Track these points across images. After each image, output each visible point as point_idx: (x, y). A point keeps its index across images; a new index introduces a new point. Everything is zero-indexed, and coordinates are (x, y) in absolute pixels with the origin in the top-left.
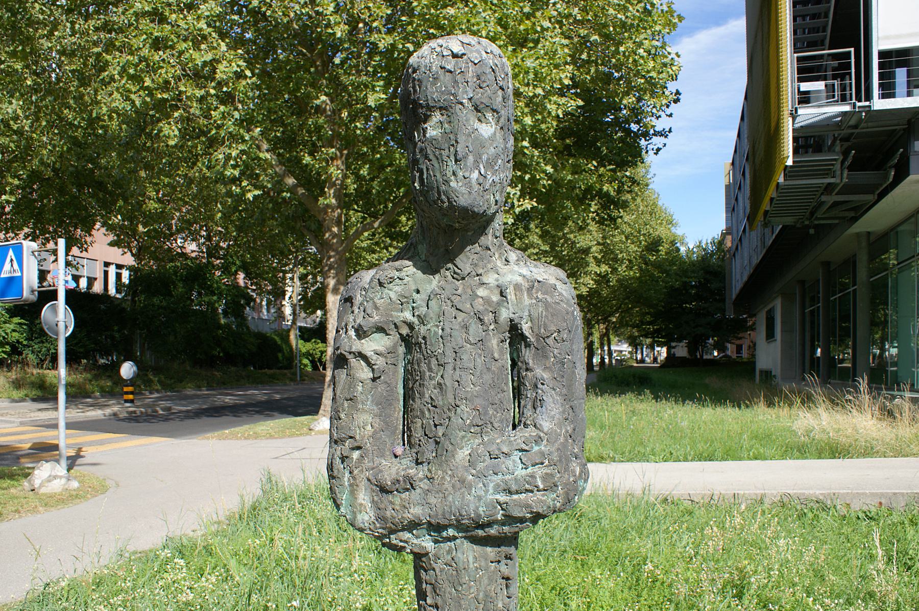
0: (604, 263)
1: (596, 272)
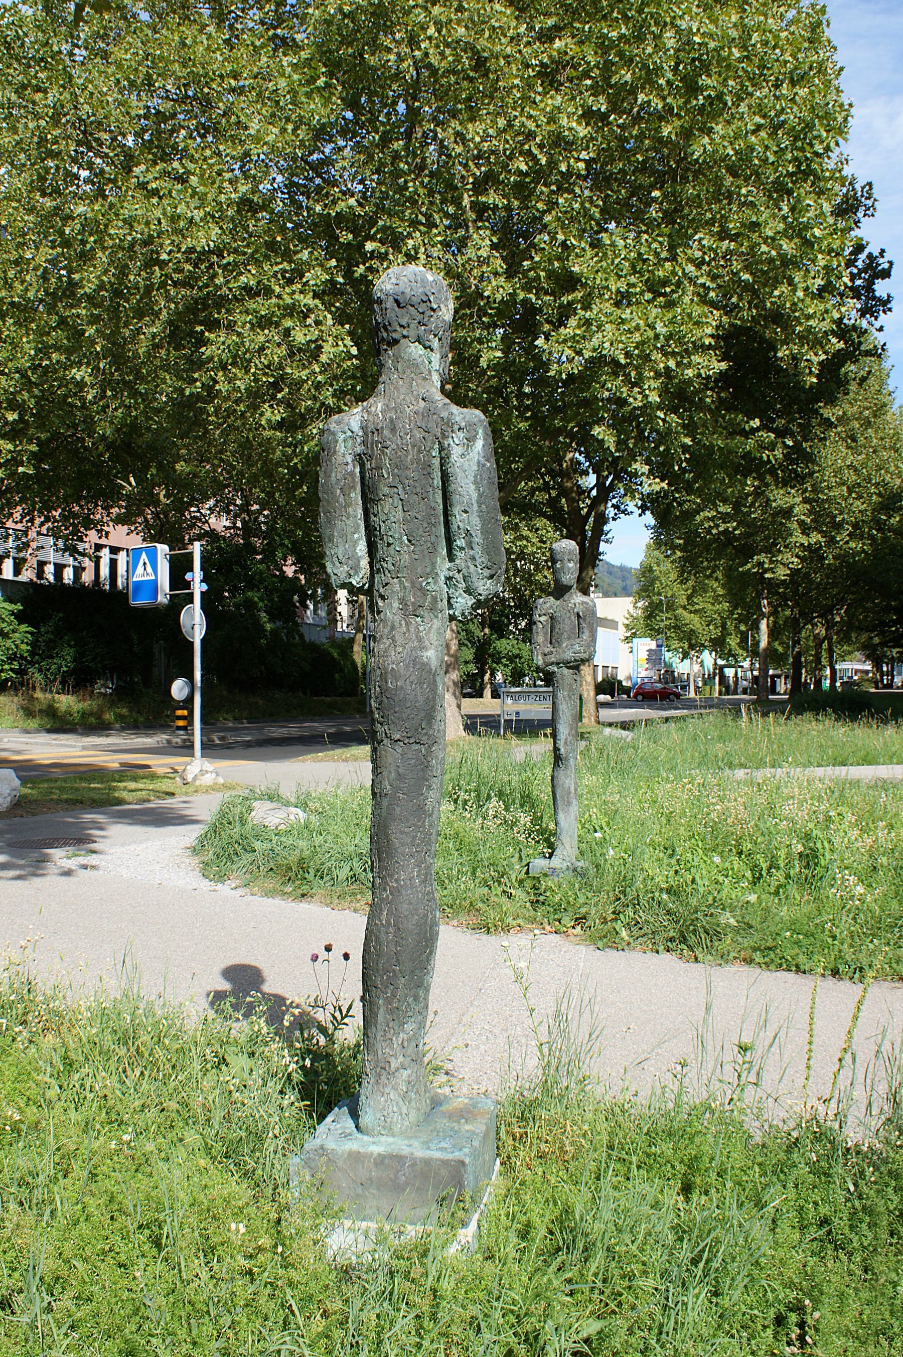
0: (816, 529)
1: (802, 544)
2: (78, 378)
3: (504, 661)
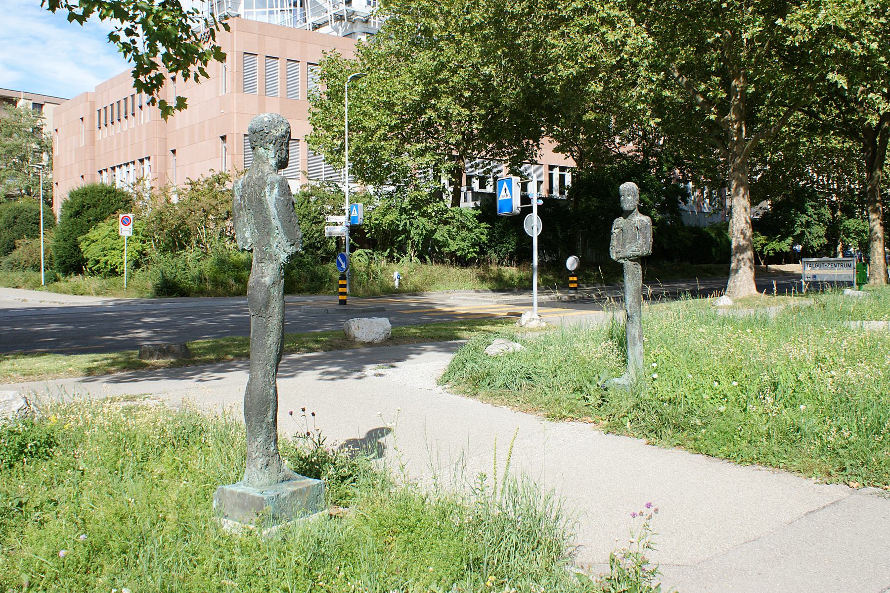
2: (487, 72)
3: (852, 235)
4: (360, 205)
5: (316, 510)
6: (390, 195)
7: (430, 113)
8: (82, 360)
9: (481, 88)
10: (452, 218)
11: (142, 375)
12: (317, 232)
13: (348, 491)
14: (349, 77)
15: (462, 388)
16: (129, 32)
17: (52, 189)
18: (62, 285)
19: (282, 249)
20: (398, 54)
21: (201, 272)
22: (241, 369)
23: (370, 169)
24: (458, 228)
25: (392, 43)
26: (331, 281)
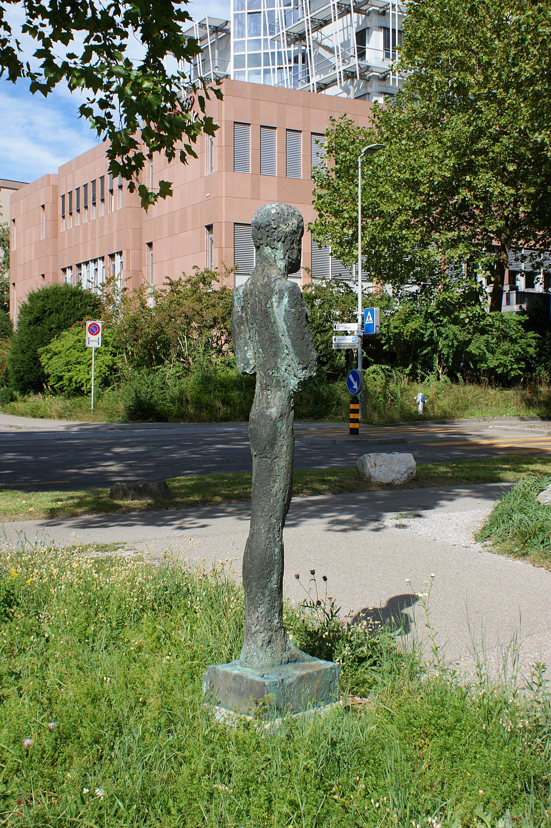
2: (539, 140)
4: (376, 309)
5: (328, 700)
6: (413, 296)
7: (465, 193)
8: (44, 499)
9: (529, 160)
10: (491, 326)
11: (113, 520)
12: (322, 343)
13: (367, 676)
14: (363, 150)
15: (507, 545)
16: (103, 104)
17: (8, 291)
18: (19, 405)
19: (292, 372)
20: (424, 119)
21: (182, 392)
22: (231, 514)
23: (387, 265)
24: (498, 338)
25: (416, 106)
26: (339, 404)
